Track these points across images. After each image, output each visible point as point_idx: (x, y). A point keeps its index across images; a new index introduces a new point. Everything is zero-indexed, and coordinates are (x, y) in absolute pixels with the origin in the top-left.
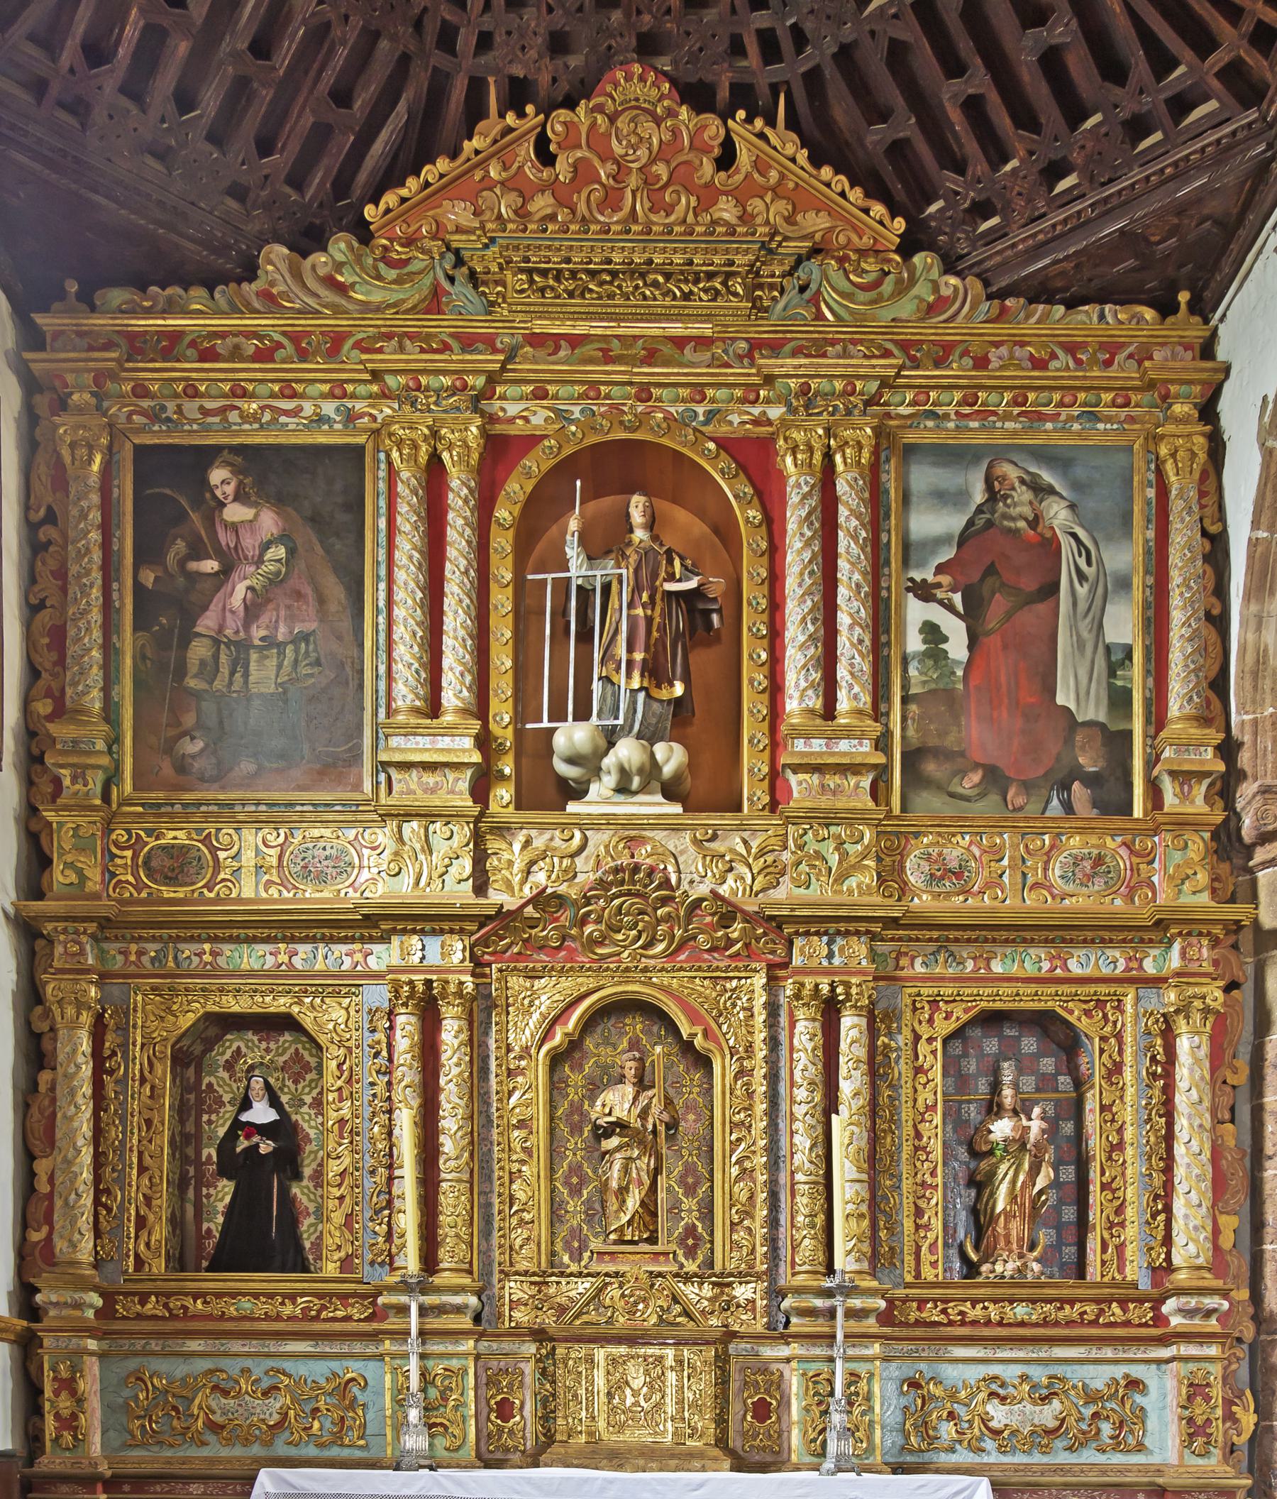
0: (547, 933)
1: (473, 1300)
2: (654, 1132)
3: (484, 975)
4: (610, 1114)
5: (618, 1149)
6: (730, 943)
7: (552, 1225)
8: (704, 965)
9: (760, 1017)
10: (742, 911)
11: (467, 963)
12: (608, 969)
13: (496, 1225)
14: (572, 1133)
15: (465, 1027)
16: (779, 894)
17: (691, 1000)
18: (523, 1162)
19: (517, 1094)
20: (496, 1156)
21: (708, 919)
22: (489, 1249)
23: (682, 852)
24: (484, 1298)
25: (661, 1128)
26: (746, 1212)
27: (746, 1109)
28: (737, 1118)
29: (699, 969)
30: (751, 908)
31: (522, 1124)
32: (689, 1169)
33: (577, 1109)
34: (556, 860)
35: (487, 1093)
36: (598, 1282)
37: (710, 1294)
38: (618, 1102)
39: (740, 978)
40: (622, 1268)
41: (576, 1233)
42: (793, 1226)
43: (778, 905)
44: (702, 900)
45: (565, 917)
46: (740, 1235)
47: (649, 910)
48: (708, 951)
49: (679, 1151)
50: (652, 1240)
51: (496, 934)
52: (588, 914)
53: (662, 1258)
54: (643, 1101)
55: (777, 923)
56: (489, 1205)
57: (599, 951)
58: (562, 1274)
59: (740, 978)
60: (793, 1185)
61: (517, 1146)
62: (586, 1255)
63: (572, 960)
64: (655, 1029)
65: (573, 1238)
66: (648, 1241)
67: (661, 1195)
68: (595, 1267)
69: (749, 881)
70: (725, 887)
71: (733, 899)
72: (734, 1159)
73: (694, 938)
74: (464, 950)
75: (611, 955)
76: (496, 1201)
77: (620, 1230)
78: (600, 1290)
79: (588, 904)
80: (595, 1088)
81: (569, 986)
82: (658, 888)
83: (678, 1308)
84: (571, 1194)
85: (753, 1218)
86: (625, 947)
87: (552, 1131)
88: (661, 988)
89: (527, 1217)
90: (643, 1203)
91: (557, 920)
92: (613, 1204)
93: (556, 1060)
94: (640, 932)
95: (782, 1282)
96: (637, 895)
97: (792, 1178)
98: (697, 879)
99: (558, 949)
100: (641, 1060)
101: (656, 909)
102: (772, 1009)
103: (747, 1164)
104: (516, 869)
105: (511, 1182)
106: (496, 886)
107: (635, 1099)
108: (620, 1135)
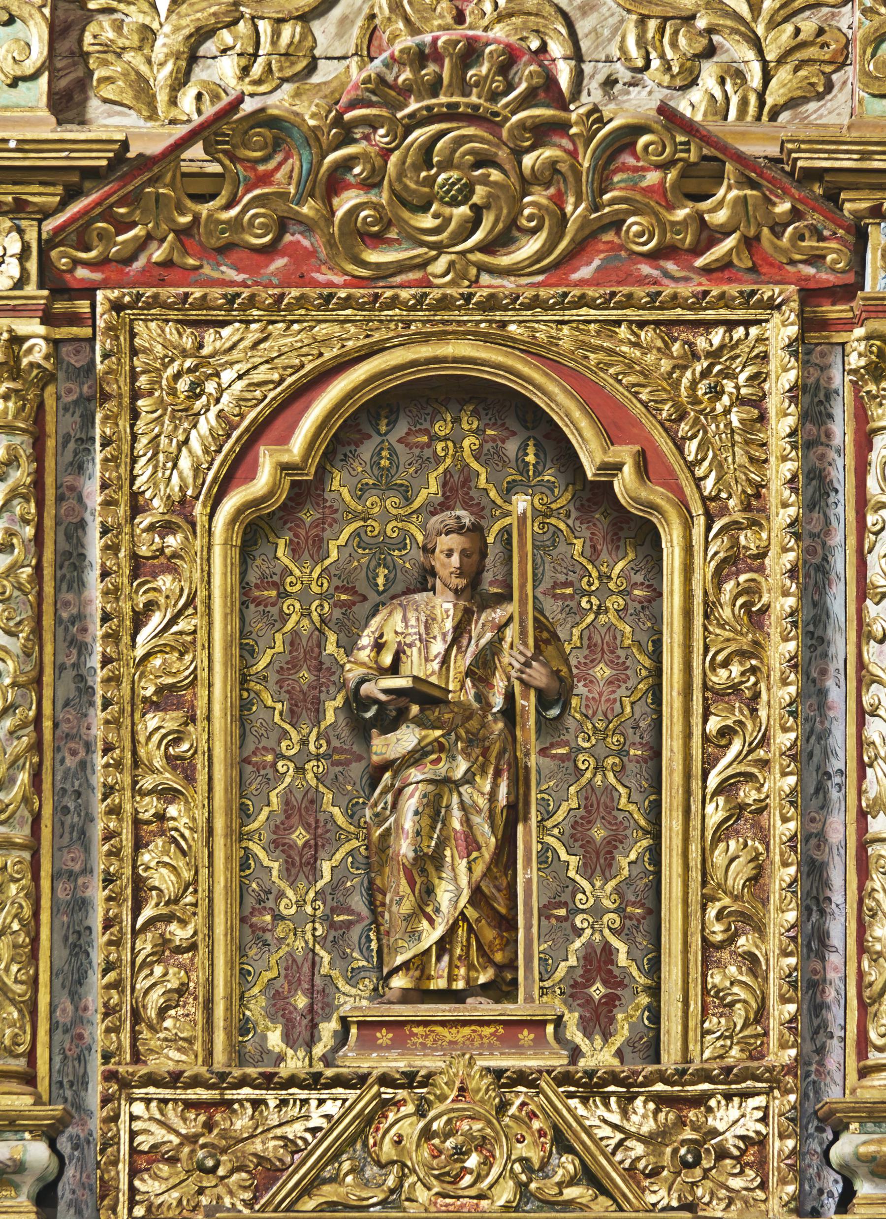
0: (241, 212)
1: (37, 1152)
2: (509, 713)
3: (74, 319)
4: (394, 669)
5: (416, 757)
6: (709, 236)
7: (242, 951)
8: (640, 292)
9: (782, 423)
10: (740, 158)
11: (31, 289)
12: (394, 303)
13: (98, 957)
14: (293, 717)
15: (24, 452)
16: (832, 113)
17: (606, 379)
18: (168, 794)
19: (156, 620)
20: (98, 779)
21: (652, 177)
22: (80, 1018)
23: (585, 10)
24: (64, 1145)
25: (527, 704)
26: (745, 917)
27: (743, 654)
28: (721, 677)
29: (629, 302)
30: (760, 147)
31: (167, 697)
32: (597, 804)
33: (305, 652)
34: (264, 27)
35: (79, 618)
36: (362, 1100)
37: (649, 1126)
38: (417, 637)
39: (731, 325)
40: (425, 1063)
41: (300, 971)
42: (862, 949)
43: (831, 143)
44: (636, 130)
45: (287, 172)
46: (728, 974)
47: (503, 154)
48: (653, 256)
49: (571, 757)
50: (502, 989)
51: (107, 215)
52: (347, 164)
53: (526, 1036)
54: (481, 635)
55: (831, 186)
56: (82, 905)
57: (373, 257)
58: (268, 1081)
59: (731, 325)
60: (862, 847)
61: (153, 753)
62: (328, 1028)
63: (303, 280)
64: (511, 447)
65: (294, 985)
66: (486, 990)
67: (527, 874)
68: (352, 1061)
69: (755, 79)
70: (696, 95)
71: (714, 127)
72: (713, 781)
73: (617, 224)
74: (23, 256)
75: (401, 267)
76: (99, 895)
77: (419, 964)
78: (368, 1121)
79: (347, 140)
80: (354, 602)
81: (291, 344)
82: (528, 100)
83: (568, 1164)
84: (290, 872)
85: (760, 930)
86: (440, 248)
87: (243, 711)
88: (530, 350)
89: (179, 933)
90: (477, 896)
91: (265, 179)
92: (400, 898)
93: (254, 530)
94: (478, 210)
95: (833, 1094)
96: (473, 117)
97: (862, 828)
98: (624, 75)
99: (268, 251)
100: (477, 531)
101: (518, 154)
102: (813, 401)
103: (748, 794)
104: (159, 51)
105: (139, 845)
106: (108, 91)
107: (461, 630)
108: (421, 723)
